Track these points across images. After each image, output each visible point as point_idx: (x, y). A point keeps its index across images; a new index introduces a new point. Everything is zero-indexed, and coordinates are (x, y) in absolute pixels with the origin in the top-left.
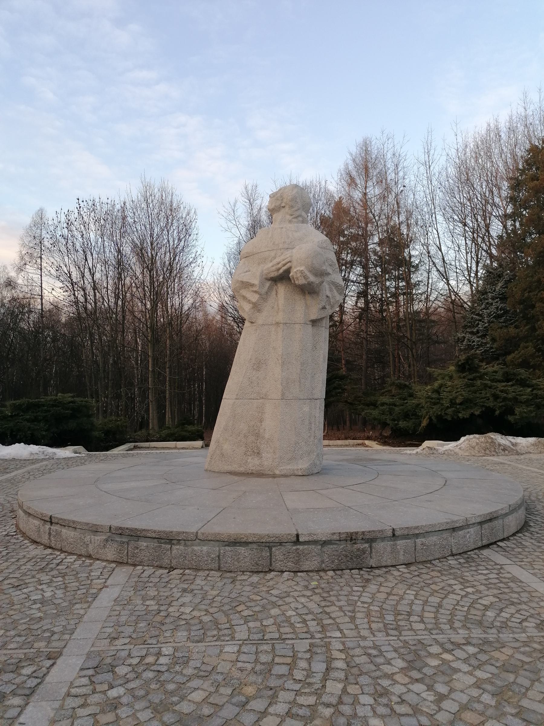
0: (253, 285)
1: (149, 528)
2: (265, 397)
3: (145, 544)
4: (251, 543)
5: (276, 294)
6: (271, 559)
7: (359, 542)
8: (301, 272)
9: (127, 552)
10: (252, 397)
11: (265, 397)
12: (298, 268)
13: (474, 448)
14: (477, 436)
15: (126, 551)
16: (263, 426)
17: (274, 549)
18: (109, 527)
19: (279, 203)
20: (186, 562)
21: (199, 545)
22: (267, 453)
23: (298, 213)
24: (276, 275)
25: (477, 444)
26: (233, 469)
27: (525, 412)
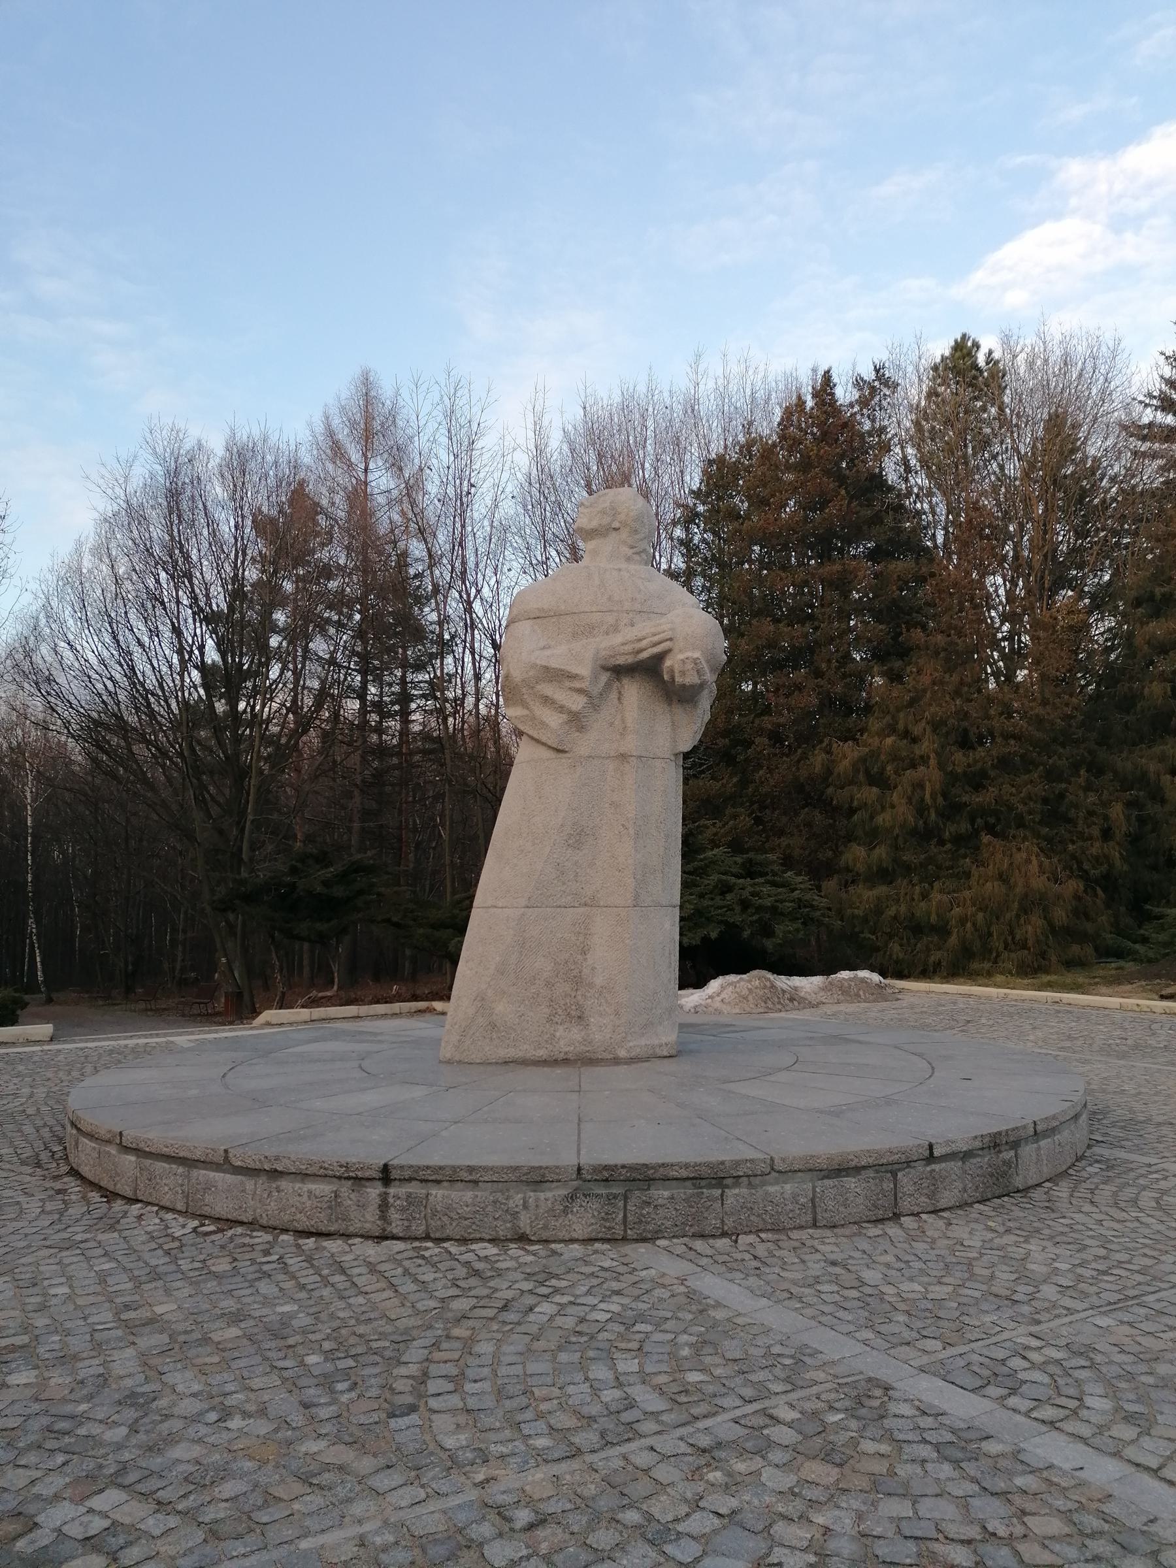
0: (573, 677)
2: (591, 903)
3: (666, 1194)
4: (864, 1168)
5: (619, 699)
6: (895, 1194)
7: (1003, 1148)
8: (695, 661)
9: (625, 1216)
11: (591, 903)
12: (689, 654)
13: (746, 998)
14: (732, 978)
15: (621, 1215)
16: (590, 962)
17: (900, 1175)
18: (575, 1169)
19: (606, 520)
21: (777, 1183)
22: (601, 1015)
24: (630, 661)
25: (750, 990)
26: (521, 1054)
27: (790, 932)
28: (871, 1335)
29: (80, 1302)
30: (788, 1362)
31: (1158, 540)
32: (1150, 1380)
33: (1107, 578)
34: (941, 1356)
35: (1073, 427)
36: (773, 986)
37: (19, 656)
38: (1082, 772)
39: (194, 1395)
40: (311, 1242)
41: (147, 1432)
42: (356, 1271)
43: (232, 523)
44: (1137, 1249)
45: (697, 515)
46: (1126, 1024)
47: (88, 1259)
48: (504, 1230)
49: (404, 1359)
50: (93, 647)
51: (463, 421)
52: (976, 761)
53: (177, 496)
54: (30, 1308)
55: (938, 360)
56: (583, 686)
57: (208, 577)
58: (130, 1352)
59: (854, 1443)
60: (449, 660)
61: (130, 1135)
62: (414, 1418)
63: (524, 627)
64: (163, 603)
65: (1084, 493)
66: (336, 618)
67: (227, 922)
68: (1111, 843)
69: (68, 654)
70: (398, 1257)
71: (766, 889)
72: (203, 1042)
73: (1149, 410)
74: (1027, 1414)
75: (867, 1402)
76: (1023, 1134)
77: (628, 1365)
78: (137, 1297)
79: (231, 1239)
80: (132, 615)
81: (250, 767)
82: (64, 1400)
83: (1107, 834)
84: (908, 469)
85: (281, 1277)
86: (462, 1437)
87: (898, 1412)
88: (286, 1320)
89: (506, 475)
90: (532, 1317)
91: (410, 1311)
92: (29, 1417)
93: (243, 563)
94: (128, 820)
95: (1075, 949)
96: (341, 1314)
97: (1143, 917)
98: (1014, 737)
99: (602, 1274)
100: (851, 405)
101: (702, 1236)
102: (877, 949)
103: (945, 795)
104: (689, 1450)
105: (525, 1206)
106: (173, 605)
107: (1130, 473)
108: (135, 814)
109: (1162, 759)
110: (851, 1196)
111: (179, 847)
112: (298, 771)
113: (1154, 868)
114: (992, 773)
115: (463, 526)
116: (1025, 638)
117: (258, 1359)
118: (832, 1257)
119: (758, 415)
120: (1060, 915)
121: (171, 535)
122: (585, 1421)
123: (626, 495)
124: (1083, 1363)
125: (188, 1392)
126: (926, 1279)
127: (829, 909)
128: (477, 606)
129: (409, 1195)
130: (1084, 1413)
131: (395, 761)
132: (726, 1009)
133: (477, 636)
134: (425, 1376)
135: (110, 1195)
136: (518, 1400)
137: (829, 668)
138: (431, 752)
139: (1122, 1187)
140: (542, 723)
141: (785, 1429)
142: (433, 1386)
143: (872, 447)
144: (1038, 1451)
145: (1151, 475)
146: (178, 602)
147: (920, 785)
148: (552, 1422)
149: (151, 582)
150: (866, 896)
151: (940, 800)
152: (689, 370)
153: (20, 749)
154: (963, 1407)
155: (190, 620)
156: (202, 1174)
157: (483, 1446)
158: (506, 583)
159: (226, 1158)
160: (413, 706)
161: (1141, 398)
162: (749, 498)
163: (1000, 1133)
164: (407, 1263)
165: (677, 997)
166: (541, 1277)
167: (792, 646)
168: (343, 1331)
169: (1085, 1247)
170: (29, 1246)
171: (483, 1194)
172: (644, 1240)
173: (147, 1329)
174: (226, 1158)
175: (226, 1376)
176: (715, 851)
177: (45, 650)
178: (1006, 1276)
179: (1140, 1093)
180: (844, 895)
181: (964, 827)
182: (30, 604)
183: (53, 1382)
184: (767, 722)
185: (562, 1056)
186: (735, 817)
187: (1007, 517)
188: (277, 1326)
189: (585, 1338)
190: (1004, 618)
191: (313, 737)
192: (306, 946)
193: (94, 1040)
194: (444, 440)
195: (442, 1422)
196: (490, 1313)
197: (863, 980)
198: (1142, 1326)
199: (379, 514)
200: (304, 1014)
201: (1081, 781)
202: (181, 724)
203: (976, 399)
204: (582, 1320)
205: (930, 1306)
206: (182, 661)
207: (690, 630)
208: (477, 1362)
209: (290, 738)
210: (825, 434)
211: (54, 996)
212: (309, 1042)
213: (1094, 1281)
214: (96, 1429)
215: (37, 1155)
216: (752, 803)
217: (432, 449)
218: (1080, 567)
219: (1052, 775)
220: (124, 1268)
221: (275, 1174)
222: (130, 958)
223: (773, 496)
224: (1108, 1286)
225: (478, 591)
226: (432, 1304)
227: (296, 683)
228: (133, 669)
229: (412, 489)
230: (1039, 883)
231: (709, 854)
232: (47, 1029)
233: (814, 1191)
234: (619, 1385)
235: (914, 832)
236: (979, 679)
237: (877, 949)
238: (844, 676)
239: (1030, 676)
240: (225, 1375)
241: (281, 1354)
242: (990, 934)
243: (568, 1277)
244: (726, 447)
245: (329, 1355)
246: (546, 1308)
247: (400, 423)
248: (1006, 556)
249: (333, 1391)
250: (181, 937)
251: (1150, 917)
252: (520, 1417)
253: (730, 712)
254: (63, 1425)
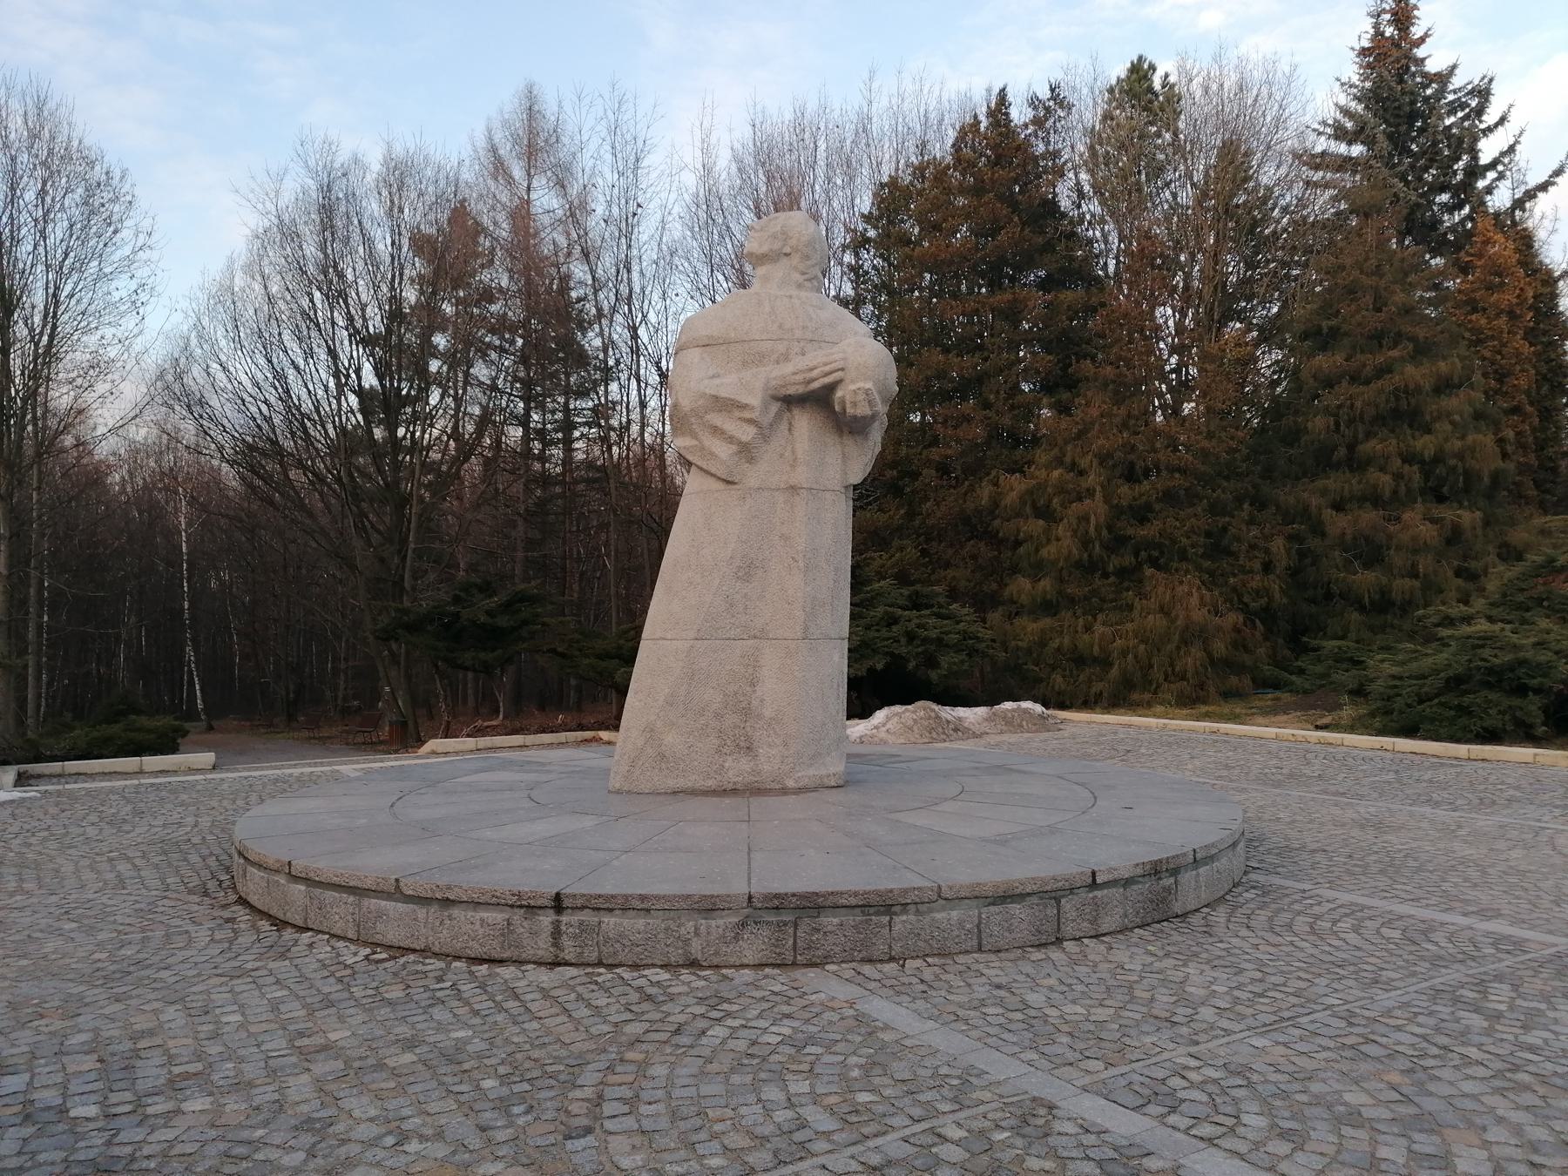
0: (744, 407)
1: (844, 889)
3: (836, 921)
4: (1029, 894)
8: (867, 392)
10: (732, 634)
12: (861, 385)
13: (911, 729)
14: (898, 708)
15: (791, 942)
16: (759, 693)
17: (1063, 901)
19: (777, 246)
20: (920, 943)
21: (943, 909)
28: (1035, 1057)
29: (253, 1029)
30: (955, 1082)
31: (1327, 273)
32: (1304, 1098)
33: (1275, 310)
34: (1103, 1076)
35: (1246, 154)
36: (938, 717)
37: (170, 378)
38: (1246, 506)
39: (371, 1120)
40: (483, 969)
41: (325, 1157)
42: (529, 997)
43: (389, 241)
44: (1290, 972)
45: (868, 240)
46: (1282, 754)
47: (260, 987)
48: (675, 956)
49: (579, 1082)
50: (247, 369)
51: (628, 137)
52: (1142, 495)
53: (330, 211)
54: (202, 1036)
55: (1114, 82)
56: (753, 416)
57: (364, 297)
58: (305, 1078)
59: (1020, 1160)
60: (614, 387)
61: (299, 865)
62: (590, 1140)
63: (693, 355)
64: (317, 325)
65: (1255, 223)
66: (497, 343)
67: (390, 650)
68: (1271, 577)
69: (220, 375)
70: (571, 983)
71: (932, 621)
72: (368, 772)
73: (1323, 138)
74: (1186, 1132)
75: (1032, 1121)
76: (1182, 861)
77: (800, 1086)
78: (310, 1024)
79: (404, 966)
80: (287, 336)
81: (411, 493)
82: (240, 1126)
83: (1267, 567)
84: (1081, 195)
85: (457, 1003)
86: (638, 1158)
87: (1062, 1130)
88: (460, 1045)
89: (673, 196)
90: (704, 1041)
91: (584, 1036)
92: (204, 1144)
93: (393, 277)
94: (286, 548)
95: (1234, 680)
96: (516, 1040)
97: (1302, 650)
98: (1179, 470)
99: (772, 998)
100: (1026, 126)
101: (870, 961)
102: (1041, 680)
103: (1110, 528)
104: (860, 1169)
105: (697, 934)
106: (329, 326)
107: (1302, 203)
108: (294, 541)
109: (1324, 492)
110: (1015, 922)
111: (338, 574)
112: (460, 498)
113: (1313, 601)
114: (1157, 507)
115: (629, 247)
116: (1193, 371)
117: (434, 1084)
118: (996, 980)
119: (930, 135)
120: (1219, 647)
121: (326, 255)
122: (758, 1142)
123: (796, 220)
124: (1240, 1082)
125: (364, 1117)
126: (1088, 1002)
127: (993, 641)
128: (642, 332)
129: (581, 923)
130: (1241, 1130)
131: (558, 489)
132: (891, 739)
133: (642, 363)
134: (600, 1099)
135: (280, 924)
136: (692, 1121)
137: (997, 398)
138: (595, 480)
139: (1279, 911)
140: (712, 454)
141: (953, 1147)
142: (608, 1109)
143: (1045, 172)
144: (1197, 1167)
145: (1322, 205)
146: (333, 324)
147: (1086, 519)
148: (726, 1142)
149: (305, 303)
150: (1030, 628)
151: (1105, 532)
152: (862, 86)
153: (172, 474)
154: (1125, 1124)
155: (346, 342)
156: (373, 903)
157: (658, 1166)
158: (671, 310)
159: (398, 887)
160: (577, 434)
161: (1316, 126)
162: (920, 223)
163: (1160, 861)
164: (579, 989)
165: (845, 728)
166: (713, 1001)
167: (962, 377)
168: (519, 1056)
169: (1241, 971)
170: (199, 975)
171: (656, 922)
172: (811, 965)
173: (321, 1056)
174: (398, 887)
175: (402, 1101)
176: (882, 583)
177: (196, 371)
178: (1165, 999)
179: (1294, 821)
180: (1008, 627)
181: (1128, 560)
182: (181, 323)
183: (228, 1109)
184: (935, 454)
185: (730, 786)
186: (901, 549)
187: (1178, 247)
188: (451, 1051)
189: (755, 1062)
190: (1173, 350)
191: (475, 465)
192: (470, 675)
193: (257, 769)
194: (608, 157)
195: (618, 1144)
196: (663, 1036)
197: (1026, 711)
198: (1296, 1046)
199: (543, 235)
200: (470, 743)
201: (1245, 515)
202: (338, 449)
203: (1151, 123)
204: (754, 1043)
205: (1092, 1028)
206: (339, 385)
207: (862, 360)
208: (651, 1084)
209: (453, 464)
210: (999, 157)
211: (215, 723)
212: (477, 772)
213: (1251, 1003)
214: (273, 1154)
215: (205, 884)
216: (919, 536)
217: (595, 164)
218: (1248, 300)
219: (1215, 509)
220: (297, 996)
221: (447, 903)
222: (292, 687)
223: (945, 221)
224: (1263, 1008)
225: (644, 316)
226: (606, 1028)
227: (457, 410)
228: (287, 392)
229: (576, 212)
230: (1199, 615)
231: (876, 586)
232: (209, 757)
233: (980, 916)
234: (790, 1104)
235: (1078, 564)
236: (1146, 412)
237: (1041, 680)
238: (1012, 407)
239: (1196, 408)
240: (401, 1100)
241: (456, 1079)
242: (1151, 666)
243: (741, 1000)
244: (897, 169)
245: (504, 1079)
246: (719, 1031)
247: (565, 140)
248: (1176, 286)
249: (509, 1115)
250: (343, 666)
251: (1306, 649)
252: (695, 1138)
253: (898, 443)
254: (240, 1150)
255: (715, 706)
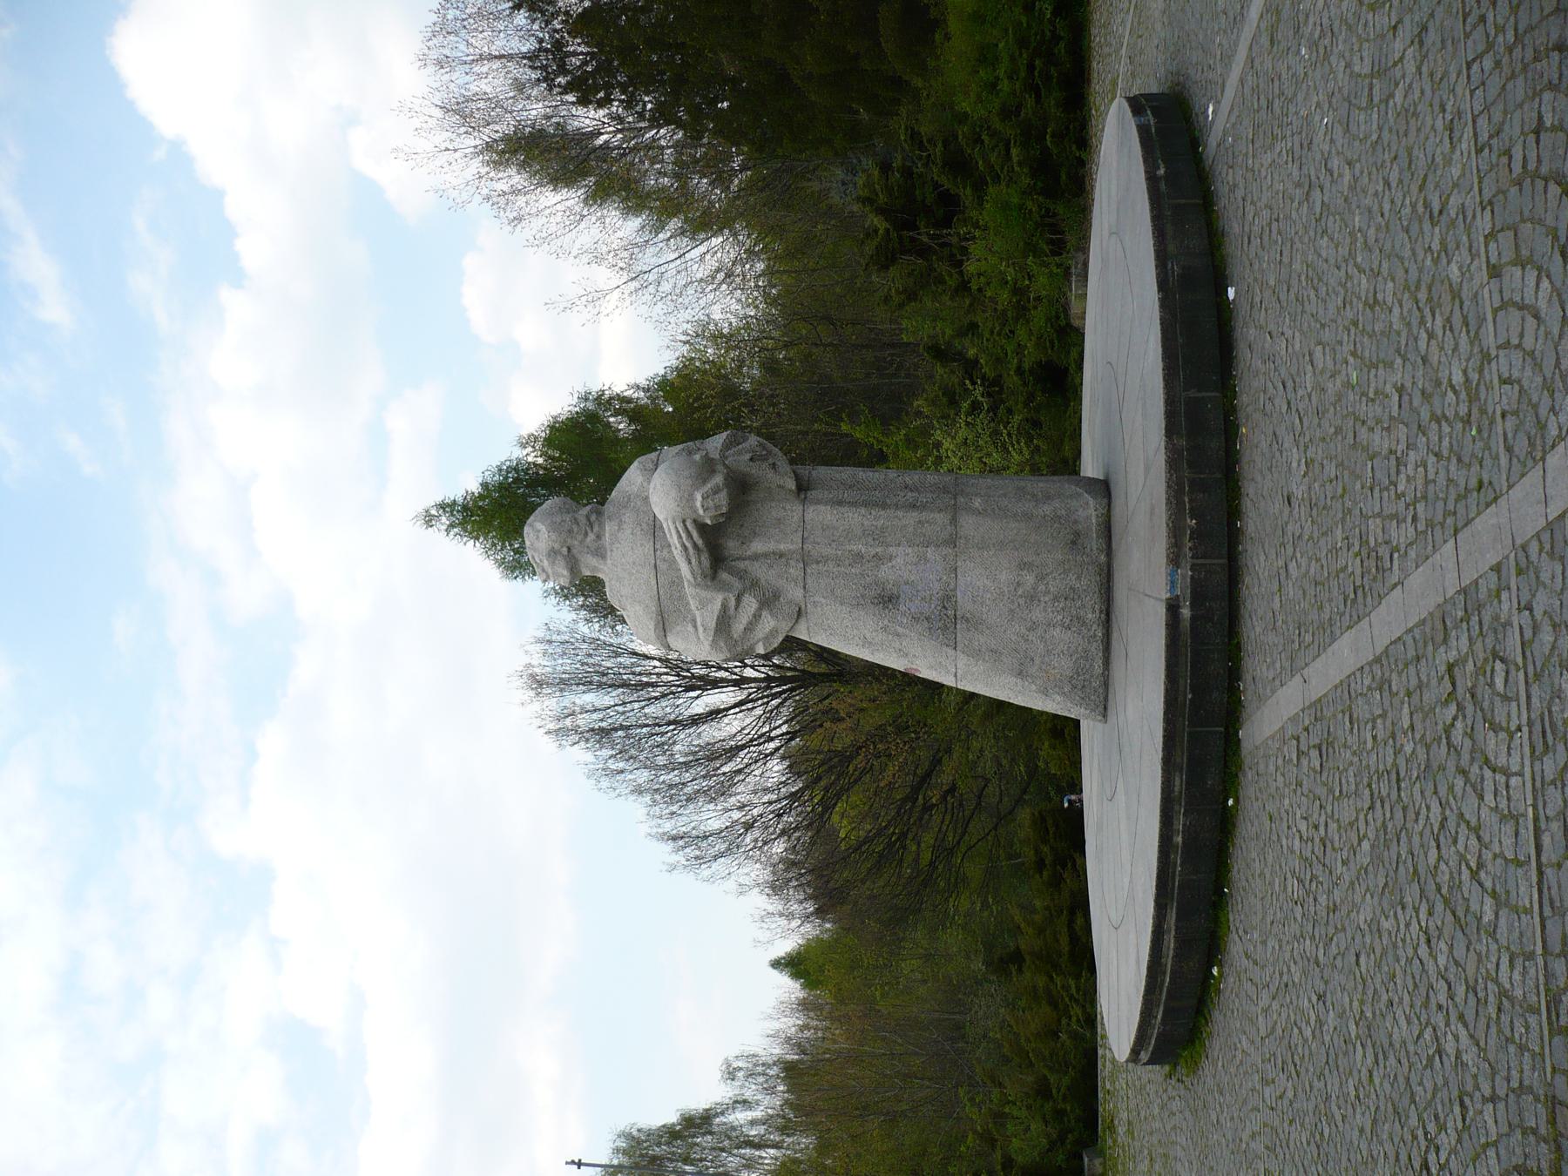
0: (724, 607)
12: (698, 504)
23: (583, 520)
255: (1023, 630)
